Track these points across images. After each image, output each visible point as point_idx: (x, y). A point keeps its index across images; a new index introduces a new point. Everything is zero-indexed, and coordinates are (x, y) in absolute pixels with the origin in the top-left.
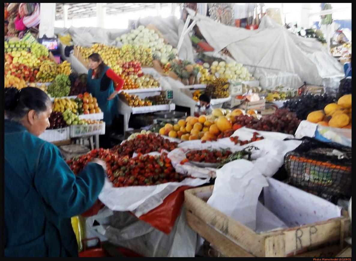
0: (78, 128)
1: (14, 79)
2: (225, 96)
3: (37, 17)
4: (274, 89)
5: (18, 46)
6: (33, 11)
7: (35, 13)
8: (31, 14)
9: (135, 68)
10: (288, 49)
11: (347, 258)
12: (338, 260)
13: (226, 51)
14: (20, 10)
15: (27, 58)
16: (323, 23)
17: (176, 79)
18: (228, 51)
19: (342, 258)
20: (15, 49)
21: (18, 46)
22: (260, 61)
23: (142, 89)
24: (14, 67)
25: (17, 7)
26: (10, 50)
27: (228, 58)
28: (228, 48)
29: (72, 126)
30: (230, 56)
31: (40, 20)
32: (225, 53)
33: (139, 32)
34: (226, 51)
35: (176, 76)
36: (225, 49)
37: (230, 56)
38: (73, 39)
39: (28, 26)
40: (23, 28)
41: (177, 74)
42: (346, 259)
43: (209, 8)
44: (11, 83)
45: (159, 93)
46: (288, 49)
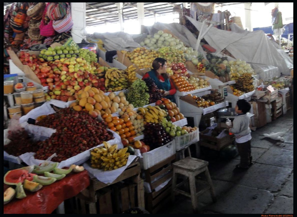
0: (182, 138)
1: (91, 89)
2: (252, 89)
3: (70, 21)
4: (272, 80)
5: (66, 52)
6: (65, 14)
7: (67, 17)
8: (62, 18)
9: (182, 69)
10: (269, 48)
11: (290, 214)
12: (282, 216)
13: (225, 51)
14: (48, 13)
15: (83, 64)
16: (275, 28)
17: (213, 78)
18: (227, 51)
19: (285, 214)
20: (63, 56)
21: (66, 52)
22: (253, 58)
23: (198, 90)
24: (79, 75)
25: (44, 8)
26: (58, 57)
27: (229, 57)
28: (227, 49)
29: (176, 137)
30: (230, 55)
31: (72, 25)
32: (225, 53)
33: (159, 36)
34: (225, 51)
35: (214, 74)
36: (225, 50)
37: (230, 55)
38: (105, 44)
39: (60, 31)
40: (51, 33)
41: (215, 73)
42: (289, 216)
43: (198, 16)
44: (90, 95)
45: (210, 92)
46: (269, 48)
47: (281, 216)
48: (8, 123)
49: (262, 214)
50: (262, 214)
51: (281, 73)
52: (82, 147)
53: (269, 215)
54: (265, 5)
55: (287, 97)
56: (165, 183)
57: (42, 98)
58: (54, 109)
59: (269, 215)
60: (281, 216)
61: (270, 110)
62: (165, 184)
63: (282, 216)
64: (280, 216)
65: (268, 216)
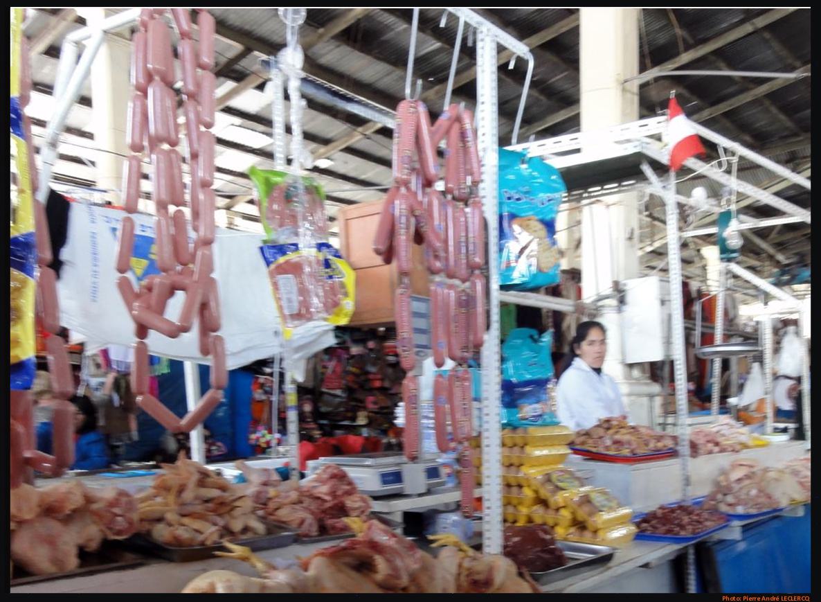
53: (745, 598)
59: (745, 598)
63: (780, 600)
65: (742, 599)
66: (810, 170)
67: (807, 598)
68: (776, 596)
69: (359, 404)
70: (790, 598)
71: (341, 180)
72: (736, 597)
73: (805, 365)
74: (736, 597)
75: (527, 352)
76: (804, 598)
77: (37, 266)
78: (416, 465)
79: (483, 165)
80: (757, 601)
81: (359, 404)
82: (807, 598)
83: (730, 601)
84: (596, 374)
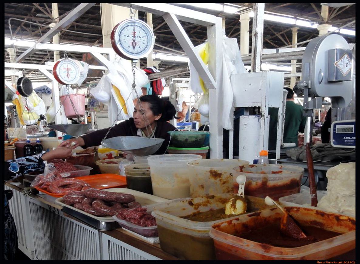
12: (342, 263)
47: (341, 263)
48: (320, 212)
49: (318, 261)
50: (318, 261)
51: (93, 105)
52: (99, 196)
53: (326, 262)
54: (14, 43)
55: (239, 33)
56: (28, 181)
57: (135, 28)
58: (322, 37)
59: (326, 262)
60: (341, 263)
61: (339, 28)
62: (281, 253)
63: (342, 263)
64: (339, 262)
65: (325, 263)
66: (102, 233)
67: (354, 262)
68: (340, 262)
69: (156, 32)
70: (346, 262)
71: (116, 101)
72: (323, 262)
73: (294, 81)
74: (323, 262)
75: (351, 154)
76: (352, 262)
77: (298, 135)
78: (47, 33)
79: (77, 85)
80: (332, 263)
81: (156, 32)
82: (354, 262)
83: (320, 263)
84: (240, 166)
